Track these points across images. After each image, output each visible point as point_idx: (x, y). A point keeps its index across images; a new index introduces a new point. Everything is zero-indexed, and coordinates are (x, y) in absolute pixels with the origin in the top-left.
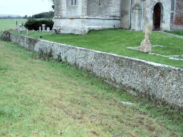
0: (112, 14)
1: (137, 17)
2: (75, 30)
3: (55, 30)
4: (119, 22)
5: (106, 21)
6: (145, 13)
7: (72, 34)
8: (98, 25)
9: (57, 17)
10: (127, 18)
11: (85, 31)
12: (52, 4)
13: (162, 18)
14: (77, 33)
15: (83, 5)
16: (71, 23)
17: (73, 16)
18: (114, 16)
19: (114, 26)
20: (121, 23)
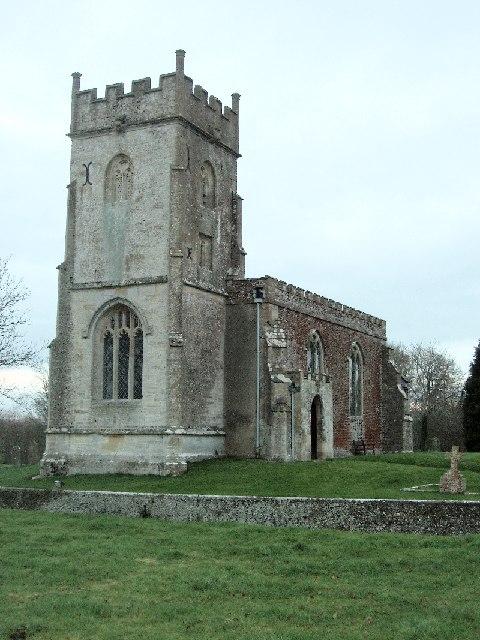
0: (212, 423)
1: (285, 428)
2: (133, 465)
3: (52, 464)
4: (221, 441)
5: (204, 439)
6: (299, 420)
7: (120, 475)
8: (193, 449)
9: (58, 430)
10: (243, 435)
11: (180, 464)
12: (454, 320)
13: (322, 430)
14: (142, 471)
15: (173, 400)
16: (112, 448)
17: (121, 424)
18: (215, 428)
19: (216, 453)
20: (227, 444)
